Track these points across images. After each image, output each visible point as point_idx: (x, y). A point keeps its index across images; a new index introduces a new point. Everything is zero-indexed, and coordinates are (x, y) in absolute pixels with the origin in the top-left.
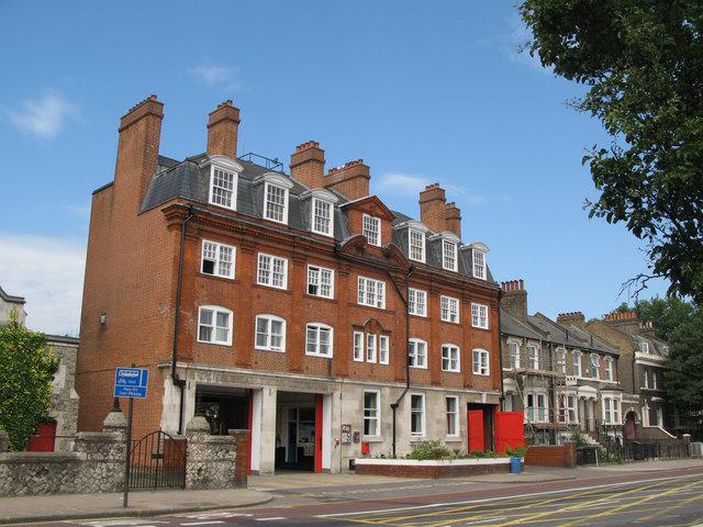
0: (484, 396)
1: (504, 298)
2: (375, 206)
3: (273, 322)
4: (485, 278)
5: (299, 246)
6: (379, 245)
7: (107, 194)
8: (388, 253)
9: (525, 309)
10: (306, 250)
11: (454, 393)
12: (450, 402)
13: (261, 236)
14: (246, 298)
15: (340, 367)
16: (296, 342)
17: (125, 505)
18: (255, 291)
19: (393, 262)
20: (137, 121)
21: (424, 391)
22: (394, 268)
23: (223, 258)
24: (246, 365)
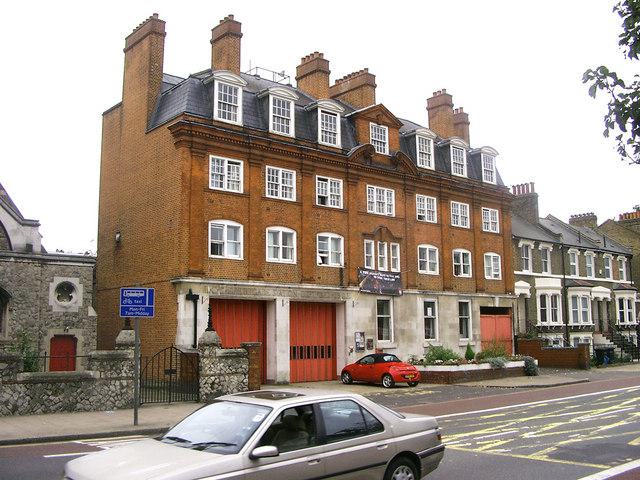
0: (497, 299)
1: (519, 204)
2: (382, 115)
3: (284, 233)
4: (494, 182)
5: (305, 155)
6: (387, 153)
7: (116, 114)
8: (395, 160)
9: (535, 211)
10: (206, 138)
11: (467, 298)
12: (463, 307)
13: (212, 138)
14: (253, 210)
15: (346, 277)
16: (307, 252)
17: (136, 423)
18: (265, 205)
19: (401, 169)
20: (140, 40)
21: (437, 297)
22: (401, 171)
23: (228, 175)
24: (258, 277)
